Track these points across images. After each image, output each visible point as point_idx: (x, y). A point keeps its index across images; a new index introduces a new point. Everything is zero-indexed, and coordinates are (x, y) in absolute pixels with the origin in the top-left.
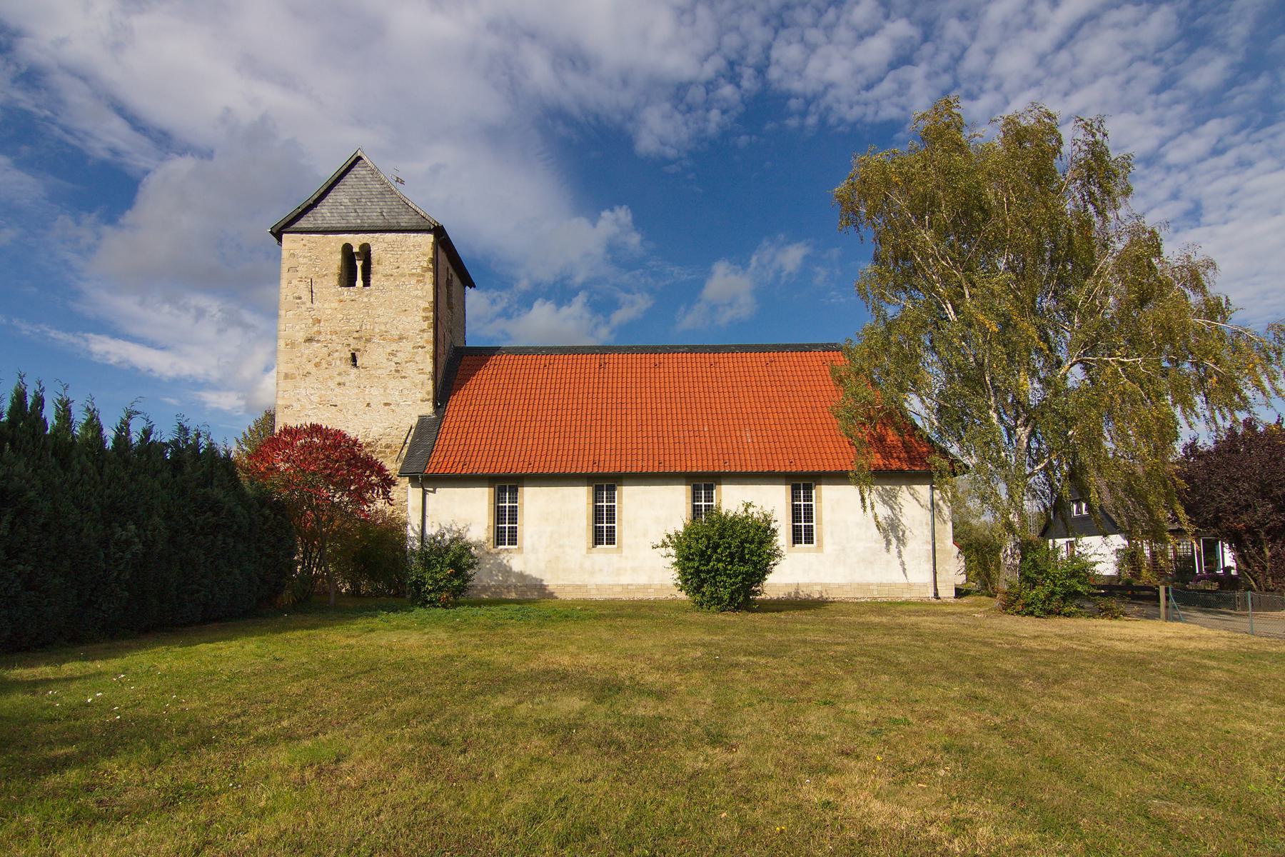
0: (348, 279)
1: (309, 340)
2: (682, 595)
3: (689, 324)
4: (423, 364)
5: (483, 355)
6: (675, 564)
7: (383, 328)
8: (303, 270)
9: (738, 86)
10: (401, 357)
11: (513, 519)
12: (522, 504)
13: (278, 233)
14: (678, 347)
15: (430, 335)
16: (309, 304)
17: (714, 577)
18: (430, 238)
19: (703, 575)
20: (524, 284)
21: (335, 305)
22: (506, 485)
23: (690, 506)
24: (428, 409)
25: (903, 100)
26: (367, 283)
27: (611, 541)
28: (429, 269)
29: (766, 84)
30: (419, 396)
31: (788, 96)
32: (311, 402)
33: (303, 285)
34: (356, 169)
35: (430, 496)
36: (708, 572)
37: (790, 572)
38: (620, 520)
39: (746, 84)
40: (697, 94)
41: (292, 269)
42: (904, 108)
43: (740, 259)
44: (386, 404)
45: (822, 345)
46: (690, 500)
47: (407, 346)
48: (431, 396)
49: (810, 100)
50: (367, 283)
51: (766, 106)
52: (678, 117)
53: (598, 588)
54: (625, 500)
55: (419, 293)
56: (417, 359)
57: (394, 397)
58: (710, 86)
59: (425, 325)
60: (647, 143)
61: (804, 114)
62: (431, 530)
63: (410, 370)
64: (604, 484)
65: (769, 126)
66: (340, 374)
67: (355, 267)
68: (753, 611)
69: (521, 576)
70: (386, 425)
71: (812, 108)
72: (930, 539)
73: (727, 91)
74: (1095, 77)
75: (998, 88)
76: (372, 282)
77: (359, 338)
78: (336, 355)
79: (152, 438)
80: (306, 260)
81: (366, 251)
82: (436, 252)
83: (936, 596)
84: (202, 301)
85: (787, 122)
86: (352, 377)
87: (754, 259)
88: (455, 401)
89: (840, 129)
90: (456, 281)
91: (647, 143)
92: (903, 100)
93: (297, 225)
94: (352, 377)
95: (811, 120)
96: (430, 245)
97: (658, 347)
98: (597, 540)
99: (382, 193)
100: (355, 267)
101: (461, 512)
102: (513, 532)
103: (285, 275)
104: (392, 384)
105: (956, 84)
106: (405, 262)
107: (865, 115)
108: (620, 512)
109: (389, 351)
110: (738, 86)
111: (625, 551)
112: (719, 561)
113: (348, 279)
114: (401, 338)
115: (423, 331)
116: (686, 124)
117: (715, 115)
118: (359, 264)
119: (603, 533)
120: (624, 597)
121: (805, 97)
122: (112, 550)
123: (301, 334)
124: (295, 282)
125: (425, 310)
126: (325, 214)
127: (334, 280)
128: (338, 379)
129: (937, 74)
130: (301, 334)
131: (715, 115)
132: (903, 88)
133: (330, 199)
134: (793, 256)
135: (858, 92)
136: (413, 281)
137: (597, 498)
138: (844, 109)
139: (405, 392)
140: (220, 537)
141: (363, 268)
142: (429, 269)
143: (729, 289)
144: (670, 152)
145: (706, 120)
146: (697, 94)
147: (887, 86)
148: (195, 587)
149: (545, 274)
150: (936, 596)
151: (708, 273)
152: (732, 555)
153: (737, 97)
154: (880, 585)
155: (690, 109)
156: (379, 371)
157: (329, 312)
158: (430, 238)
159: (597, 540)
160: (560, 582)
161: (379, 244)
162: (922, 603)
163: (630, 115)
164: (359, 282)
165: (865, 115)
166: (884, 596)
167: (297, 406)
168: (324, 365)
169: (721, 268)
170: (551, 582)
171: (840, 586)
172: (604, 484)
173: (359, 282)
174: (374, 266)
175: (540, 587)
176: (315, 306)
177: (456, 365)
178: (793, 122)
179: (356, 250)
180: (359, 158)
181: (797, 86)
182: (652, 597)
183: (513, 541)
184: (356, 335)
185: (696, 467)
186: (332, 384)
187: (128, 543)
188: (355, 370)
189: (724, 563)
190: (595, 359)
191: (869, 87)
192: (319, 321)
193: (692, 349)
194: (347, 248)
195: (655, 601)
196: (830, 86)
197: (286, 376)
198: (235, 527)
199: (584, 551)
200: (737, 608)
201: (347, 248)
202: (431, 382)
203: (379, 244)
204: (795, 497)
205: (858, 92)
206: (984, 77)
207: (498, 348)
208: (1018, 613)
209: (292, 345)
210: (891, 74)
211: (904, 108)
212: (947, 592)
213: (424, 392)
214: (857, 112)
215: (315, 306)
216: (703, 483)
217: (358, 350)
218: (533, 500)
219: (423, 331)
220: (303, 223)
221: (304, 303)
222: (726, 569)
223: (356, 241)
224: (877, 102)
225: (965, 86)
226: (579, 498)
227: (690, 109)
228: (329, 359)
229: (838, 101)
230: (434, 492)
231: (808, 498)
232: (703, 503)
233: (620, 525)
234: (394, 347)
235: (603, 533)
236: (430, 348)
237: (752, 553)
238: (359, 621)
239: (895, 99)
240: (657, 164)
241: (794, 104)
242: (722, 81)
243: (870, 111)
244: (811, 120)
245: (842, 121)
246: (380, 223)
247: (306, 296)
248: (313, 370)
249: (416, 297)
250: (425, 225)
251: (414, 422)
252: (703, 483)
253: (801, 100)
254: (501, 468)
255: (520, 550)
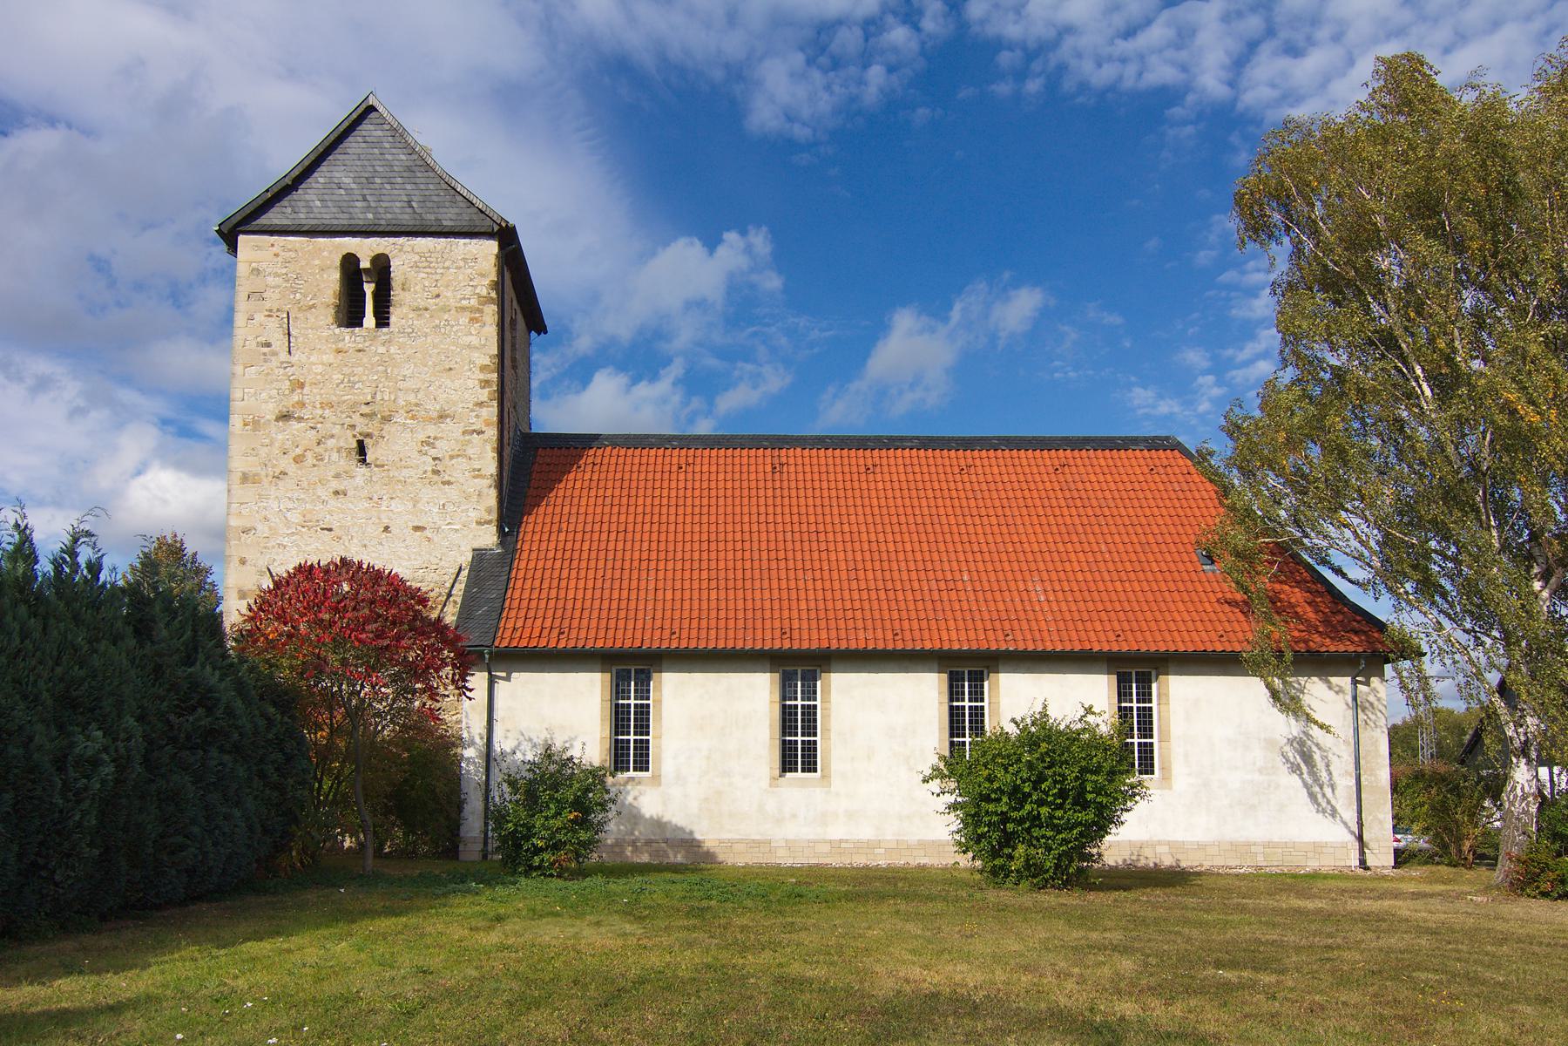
0: (350, 315)
1: (285, 417)
2: (965, 861)
3: (839, 413)
4: (484, 457)
5: (573, 447)
6: (953, 807)
7: (412, 398)
8: (273, 299)
9: (917, 28)
10: (443, 448)
11: (643, 728)
12: (659, 702)
13: (229, 236)
14: (902, 439)
15: (491, 412)
16: (284, 356)
17: (1028, 831)
18: (492, 247)
19: (1010, 827)
20: (584, 344)
21: (329, 357)
22: (631, 669)
23: (777, 708)
24: (488, 538)
25: (1183, 55)
26: (382, 320)
27: (810, 766)
28: (489, 300)
29: (963, 26)
30: (474, 515)
31: (998, 44)
32: (288, 523)
33: (273, 324)
34: (366, 128)
35: (501, 686)
36: (1021, 821)
37: (1151, 826)
38: (826, 730)
39: (928, 24)
40: (848, 40)
41: (256, 295)
42: (1184, 68)
43: (935, 306)
44: (417, 528)
45: (1145, 439)
46: (777, 697)
47: (452, 430)
48: (494, 516)
49: (1035, 52)
50: (382, 320)
51: (961, 59)
52: (816, 75)
53: (790, 845)
54: (835, 696)
55: (474, 340)
56: (470, 451)
57: (431, 516)
58: (872, 27)
59: (484, 395)
60: (763, 116)
61: (1021, 75)
62: (502, 743)
63: (458, 470)
64: (800, 668)
65: (966, 93)
66: (337, 476)
67: (364, 295)
68: (1091, 887)
69: (658, 824)
70: (417, 564)
71: (1036, 66)
72: (1352, 767)
73: (899, 35)
74: (1495, 24)
75: (1337, 38)
76: (393, 319)
77: (371, 416)
78: (331, 443)
79: (102, 577)
80: (278, 281)
81: (382, 267)
82: (501, 273)
83: (1363, 863)
84: (41, 366)
85: (994, 87)
86: (359, 481)
87: (958, 307)
88: (533, 524)
89: (1080, 100)
90: (521, 324)
91: (763, 116)
92: (1183, 55)
93: (264, 220)
94: (359, 481)
95: (1033, 86)
96: (493, 260)
97: (868, 439)
98: (787, 765)
99: (409, 169)
100: (364, 295)
101: (544, 714)
102: (643, 748)
103: (242, 307)
104: (427, 493)
105: (1270, 32)
106: (446, 282)
107: (1121, 78)
108: (826, 717)
109: (422, 437)
110: (917, 28)
111: (836, 780)
112: (1041, 803)
113: (350, 315)
114: (442, 417)
115: (481, 404)
116: (828, 88)
117: (876, 73)
118: (369, 289)
119: (798, 751)
120: (835, 861)
121: (1025, 49)
122: (72, 773)
123: (271, 406)
124: (260, 317)
125: (483, 368)
126: (311, 202)
127: (326, 316)
128: (335, 485)
129: (1240, 14)
130: (271, 406)
131: (876, 73)
132: (1184, 36)
133: (320, 177)
134: (1021, 307)
135: (1111, 43)
136: (464, 320)
137: (786, 692)
138: (1087, 66)
139: (450, 508)
140: (214, 752)
141: (376, 295)
142: (489, 300)
143: (913, 360)
144: (801, 133)
145: (861, 82)
146: (848, 40)
147: (1158, 33)
148: (179, 839)
149: (621, 326)
150: (1363, 863)
151: (881, 329)
152: (1063, 794)
153: (914, 45)
154: (1269, 845)
155: (836, 64)
156: (405, 472)
157: (319, 369)
158: (492, 247)
159: (787, 765)
160: (726, 836)
161: (405, 255)
162: (1341, 876)
163: (739, 73)
164: (369, 320)
165: (1121, 78)
166: (1274, 862)
167: (262, 529)
168: (310, 459)
169: (904, 321)
170: (708, 834)
171: (1201, 847)
172: (800, 668)
173: (369, 320)
174: (396, 294)
175: (690, 844)
176: (294, 359)
177: (532, 467)
178: (1003, 89)
179: (365, 264)
180: (372, 109)
181: (1013, 30)
182: (883, 863)
183: (642, 764)
184: (366, 410)
185: (958, 641)
186: (324, 493)
187: (95, 763)
188: (364, 469)
189: (1040, 813)
190: (765, 457)
191: (1130, 33)
192: (302, 386)
193: (926, 443)
194: (350, 262)
195: (889, 869)
196: (1068, 30)
197: (245, 478)
198: (236, 736)
199: (765, 783)
200: (1066, 884)
201: (350, 262)
202: (493, 493)
203: (405, 255)
204: (954, 693)
205: (1111, 43)
206: (1315, 21)
207: (596, 437)
208: (1545, 895)
209: (255, 424)
210: (1166, 15)
211: (1184, 68)
212: (1382, 858)
213: (482, 507)
214: (1107, 74)
215: (294, 359)
216: (967, 671)
217: (369, 435)
218: (678, 697)
219: (481, 404)
220: (273, 218)
221: (275, 354)
222: (1051, 817)
223: (365, 249)
224: (1142, 57)
225: (1283, 34)
226: (757, 692)
227: (836, 64)
228: (319, 449)
229: (1079, 55)
230: (508, 679)
231: (1145, 696)
232: (967, 704)
233: (826, 738)
234: (431, 430)
235: (798, 751)
236: (492, 433)
237: (1098, 791)
238: (455, 900)
239: (1170, 54)
240: (780, 148)
241: (1005, 58)
242: (890, 19)
243: (1131, 70)
244: (1033, 86)
245: (1083, 87)
246: (406, 219)
247: (279, 341)
248: (292, 469)
249: (469, 346)
250: (486, 225)
251: (466, 558)
252: (967, 671)
253: (1019, 53)
254: (625, 639)
255: (657, 779)
